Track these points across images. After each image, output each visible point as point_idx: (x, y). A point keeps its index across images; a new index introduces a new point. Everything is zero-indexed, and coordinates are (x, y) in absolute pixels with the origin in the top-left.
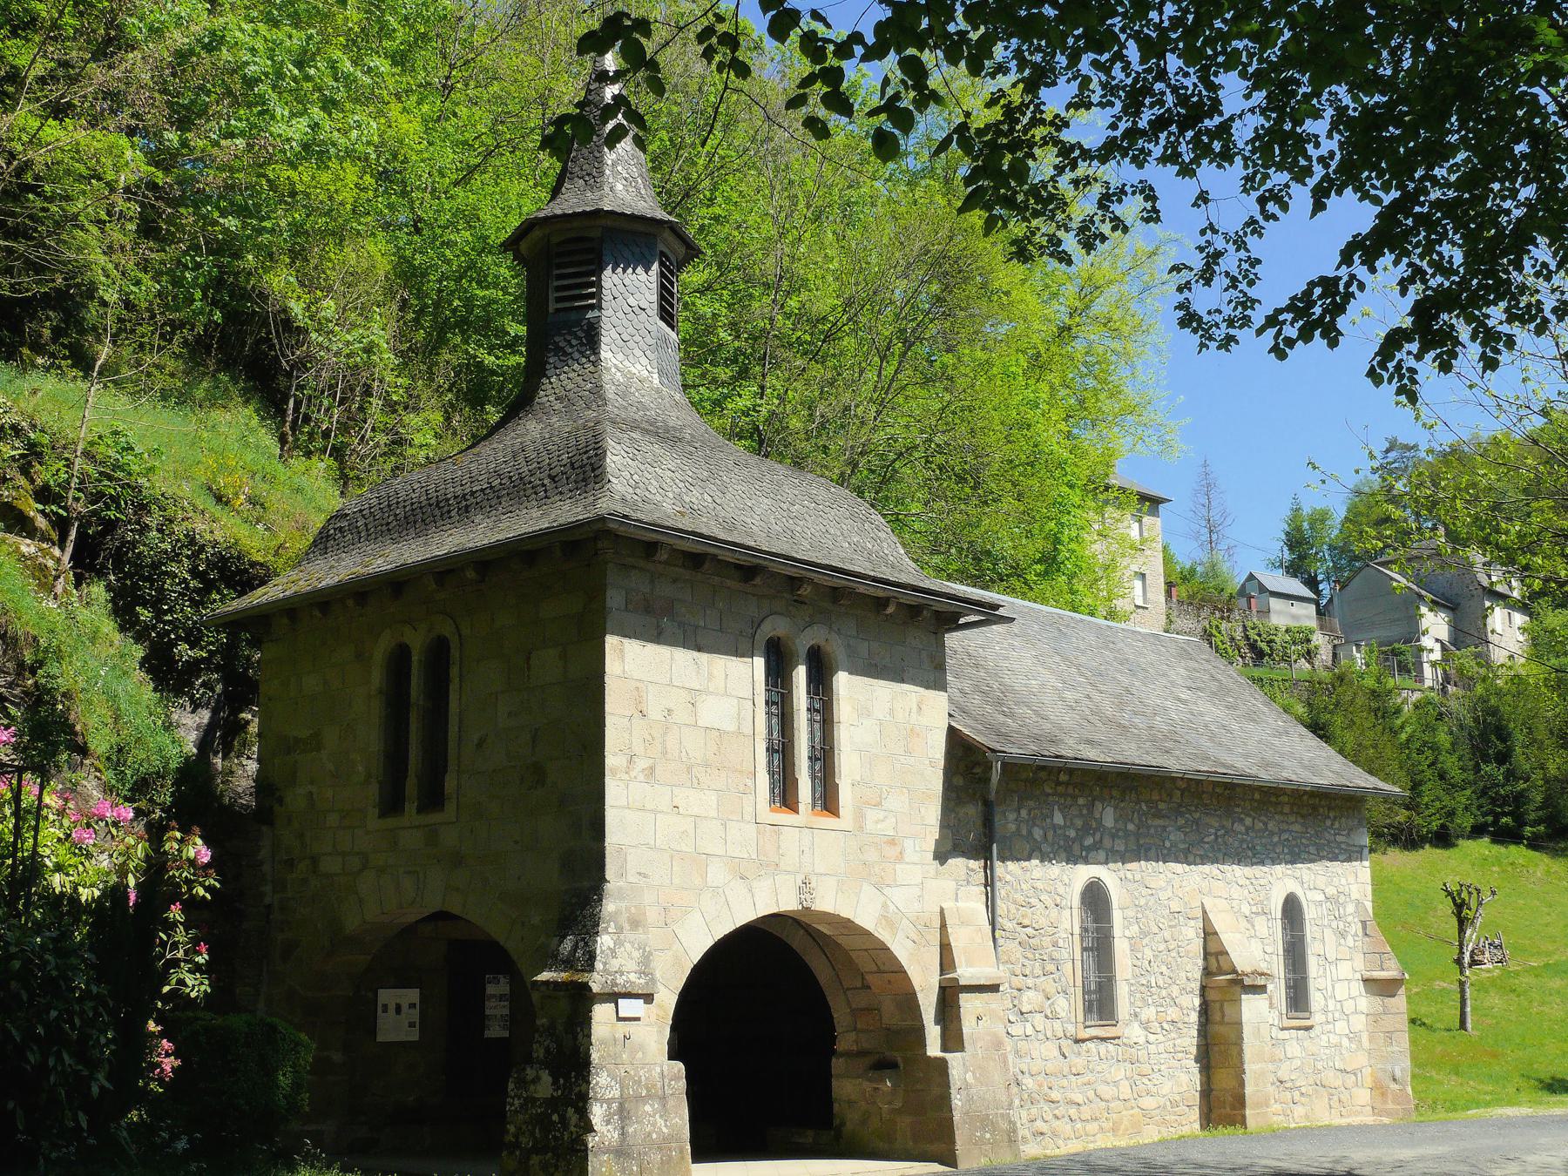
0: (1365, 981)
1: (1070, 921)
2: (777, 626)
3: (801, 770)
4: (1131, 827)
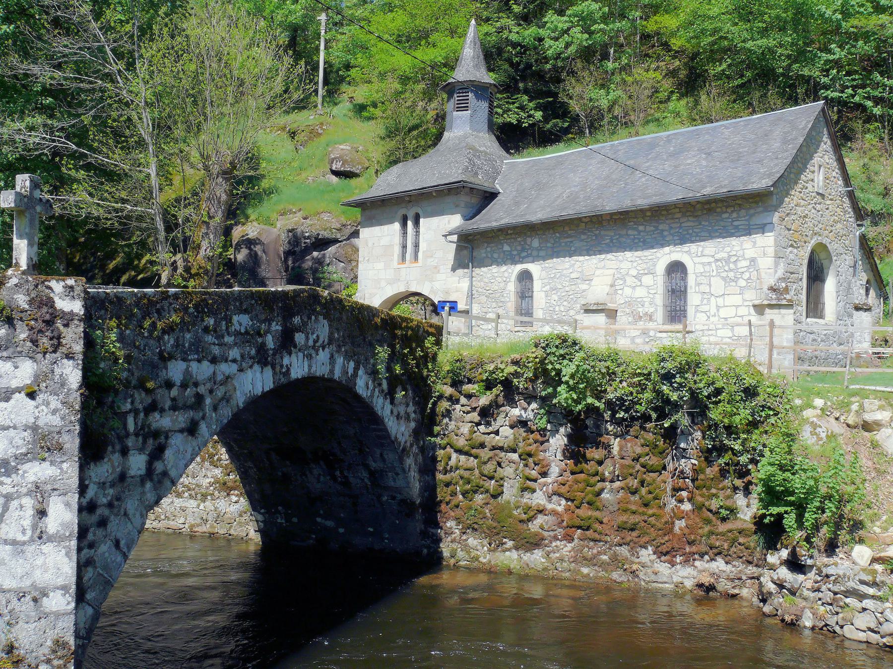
0: (754, 306)
1: (512, 287)
2: (403, 211)
3: (409, 251)
4: (549, 245)
